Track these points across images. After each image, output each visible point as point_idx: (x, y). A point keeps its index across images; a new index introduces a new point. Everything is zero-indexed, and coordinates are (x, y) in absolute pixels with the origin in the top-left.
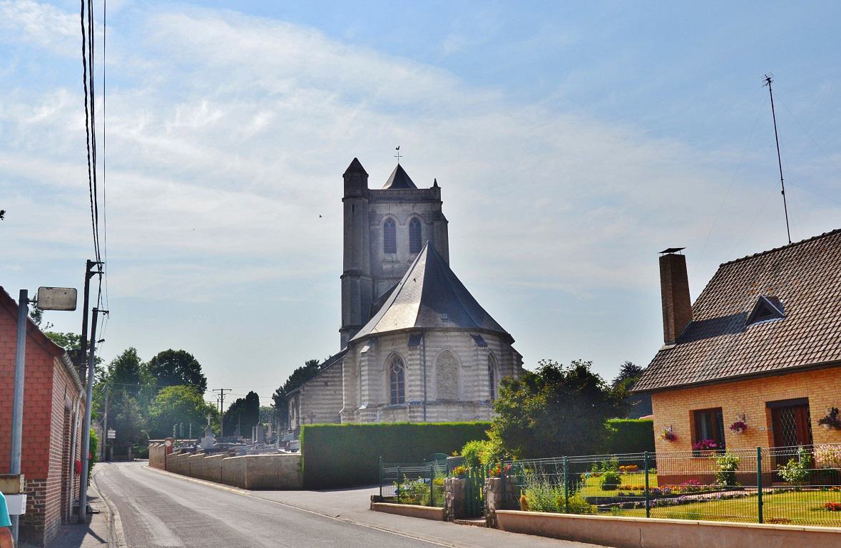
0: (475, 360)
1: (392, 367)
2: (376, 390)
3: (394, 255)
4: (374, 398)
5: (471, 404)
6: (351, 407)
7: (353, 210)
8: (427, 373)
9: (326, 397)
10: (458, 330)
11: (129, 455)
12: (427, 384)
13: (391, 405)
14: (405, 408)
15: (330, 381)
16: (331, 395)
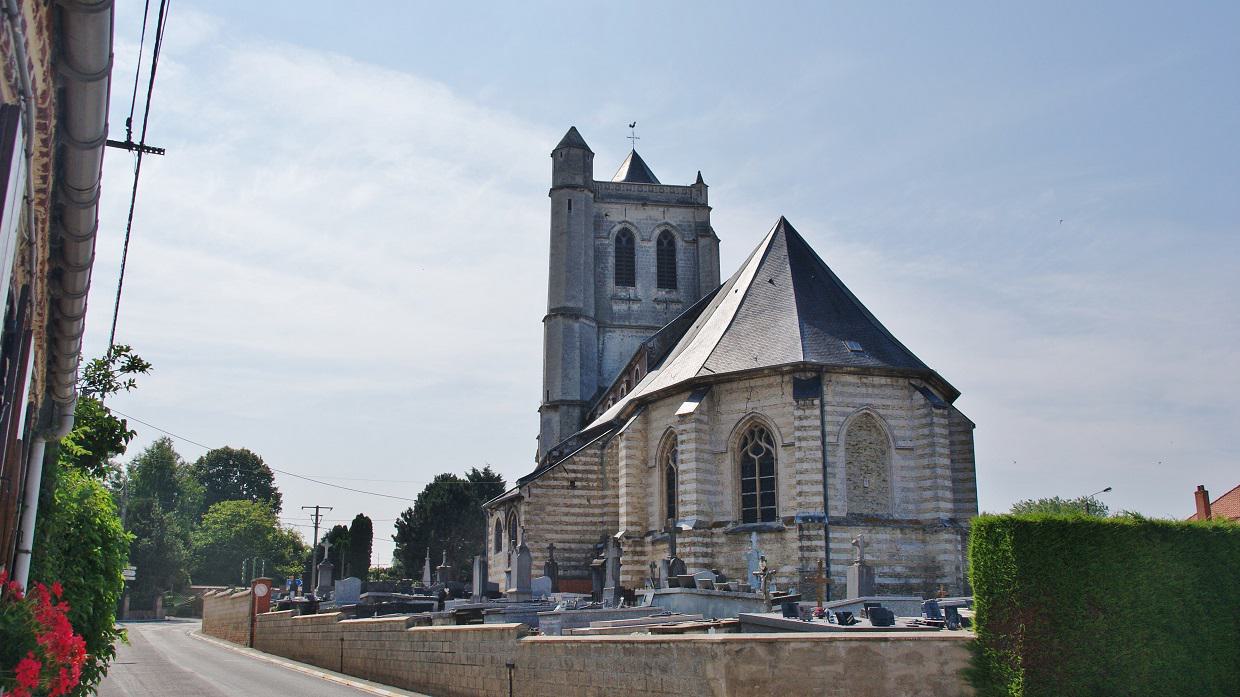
0: (925, 436)
1: (745, 444)
2: (709, 492)
3: (631, 290)
4: (706, 508)
5: (916, 525)
6: (638, 528)
7: (570, 208)
8: (830, 459)
9: (573, 510)
10: (889, 374)
11: (158, 610)
12: (830, 481)
13: (741, 525)
14: (781, 530)
15: (581, 480)
16: (580, 506)
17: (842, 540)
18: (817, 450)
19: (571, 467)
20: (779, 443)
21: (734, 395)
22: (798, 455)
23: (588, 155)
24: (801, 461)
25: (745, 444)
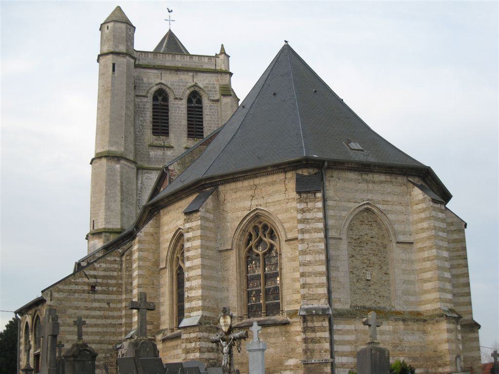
8: (332, 252)
12: (333, 274)
14: (286, 324)
15: (101, 285)
16: (100, 309)
17: (348, 332)
18: (320, 242)
19: (92, 273)
20: (283, 238)
21: (239, 194)
22: (301, 247)
23: (131, 28)
24: (304, 253)
25: (250, 239)
